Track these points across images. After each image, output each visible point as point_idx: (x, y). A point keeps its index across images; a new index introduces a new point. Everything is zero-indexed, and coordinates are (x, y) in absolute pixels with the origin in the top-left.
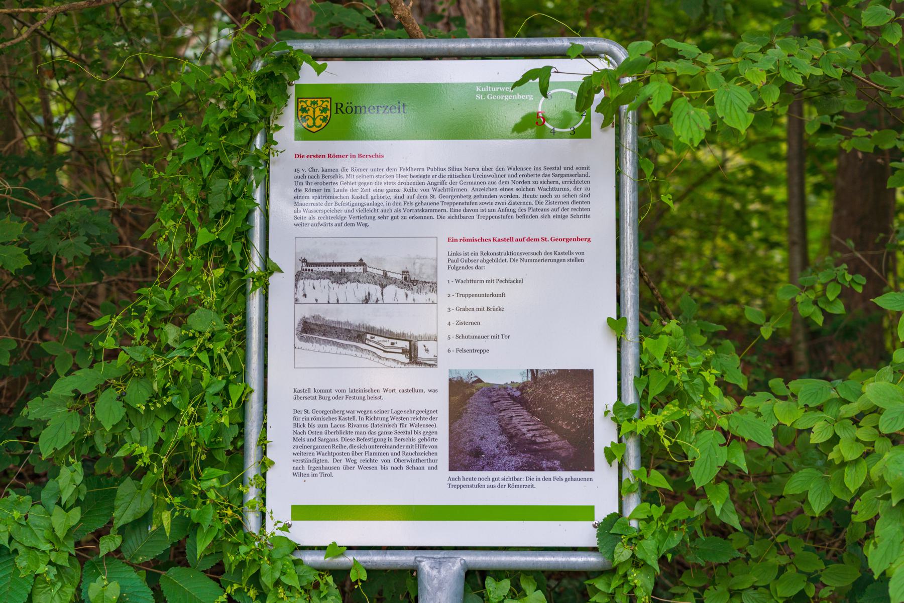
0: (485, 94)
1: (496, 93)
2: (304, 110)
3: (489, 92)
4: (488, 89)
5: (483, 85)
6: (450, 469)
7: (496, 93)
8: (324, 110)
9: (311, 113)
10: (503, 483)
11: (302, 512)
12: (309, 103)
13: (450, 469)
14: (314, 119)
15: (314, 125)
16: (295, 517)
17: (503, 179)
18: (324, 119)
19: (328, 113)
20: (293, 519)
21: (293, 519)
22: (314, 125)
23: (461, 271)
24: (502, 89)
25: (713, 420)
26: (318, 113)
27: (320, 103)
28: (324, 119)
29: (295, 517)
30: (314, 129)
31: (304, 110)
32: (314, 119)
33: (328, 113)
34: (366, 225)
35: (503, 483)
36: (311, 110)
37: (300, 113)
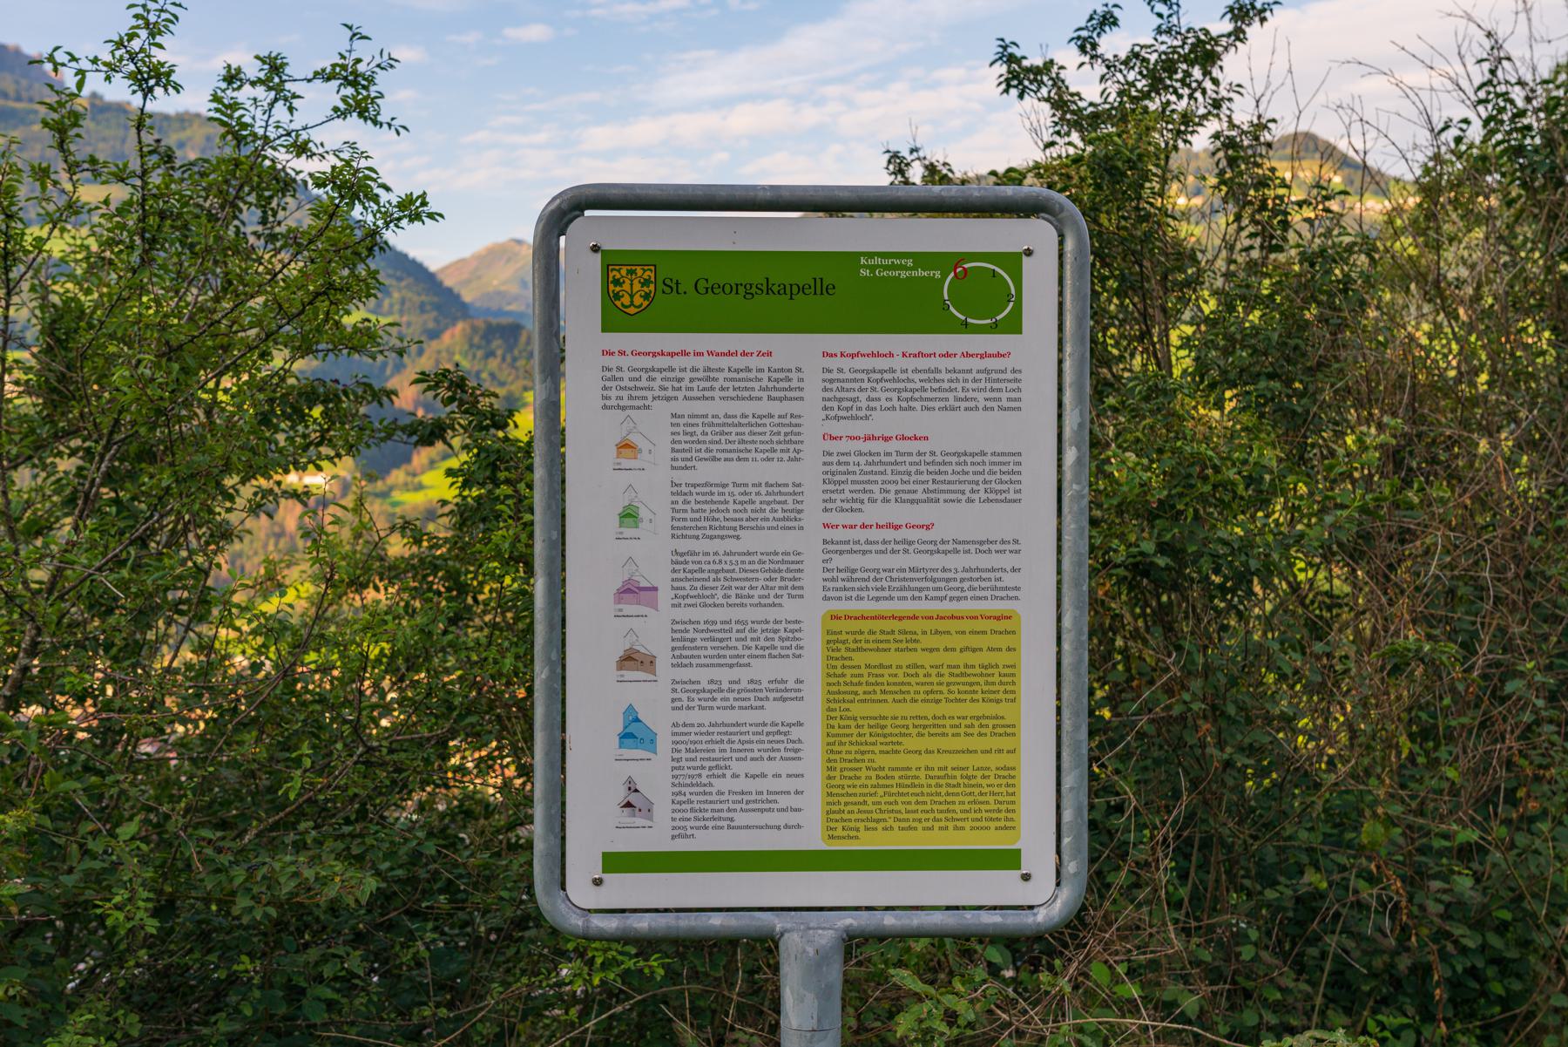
0: (872, 268)
1: (887, 268)
2: (617, 282)
3: (878, 266)
4: (877, 261)
5: (871, 255)
6: (606, 328)
7: (887, 268)
8: (646, 283)
9: (626, 286)
10: (897, 547)
11: (615, 862)
12: (624, 272)
13: (606, 328)
14: (632, 296)
15: (632, 304)
16: (607, 868)
17: (921, 799)
18: (646, 296)
19: (652, 287)
20: (604, 871)
21: (604, 871)
22: (632, 304)
23: (845, 556)
24: (897, 262)
25: (1135, 965)
26: (637, 286)
27: (639, 271)
28: (646, 296)
29: (607, 868)
30: (632, 310)
31: (617, 282)
32: (632, 296)
33: (652, 287)
34: (738, 538)
35: (897, 547)
36: (628, 282)
37: (611, 287)
